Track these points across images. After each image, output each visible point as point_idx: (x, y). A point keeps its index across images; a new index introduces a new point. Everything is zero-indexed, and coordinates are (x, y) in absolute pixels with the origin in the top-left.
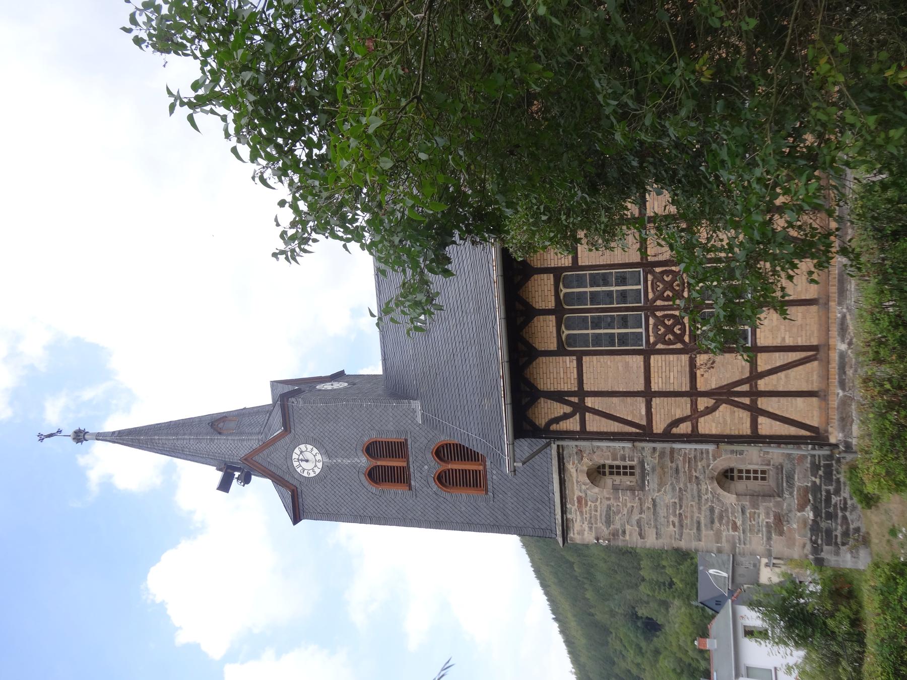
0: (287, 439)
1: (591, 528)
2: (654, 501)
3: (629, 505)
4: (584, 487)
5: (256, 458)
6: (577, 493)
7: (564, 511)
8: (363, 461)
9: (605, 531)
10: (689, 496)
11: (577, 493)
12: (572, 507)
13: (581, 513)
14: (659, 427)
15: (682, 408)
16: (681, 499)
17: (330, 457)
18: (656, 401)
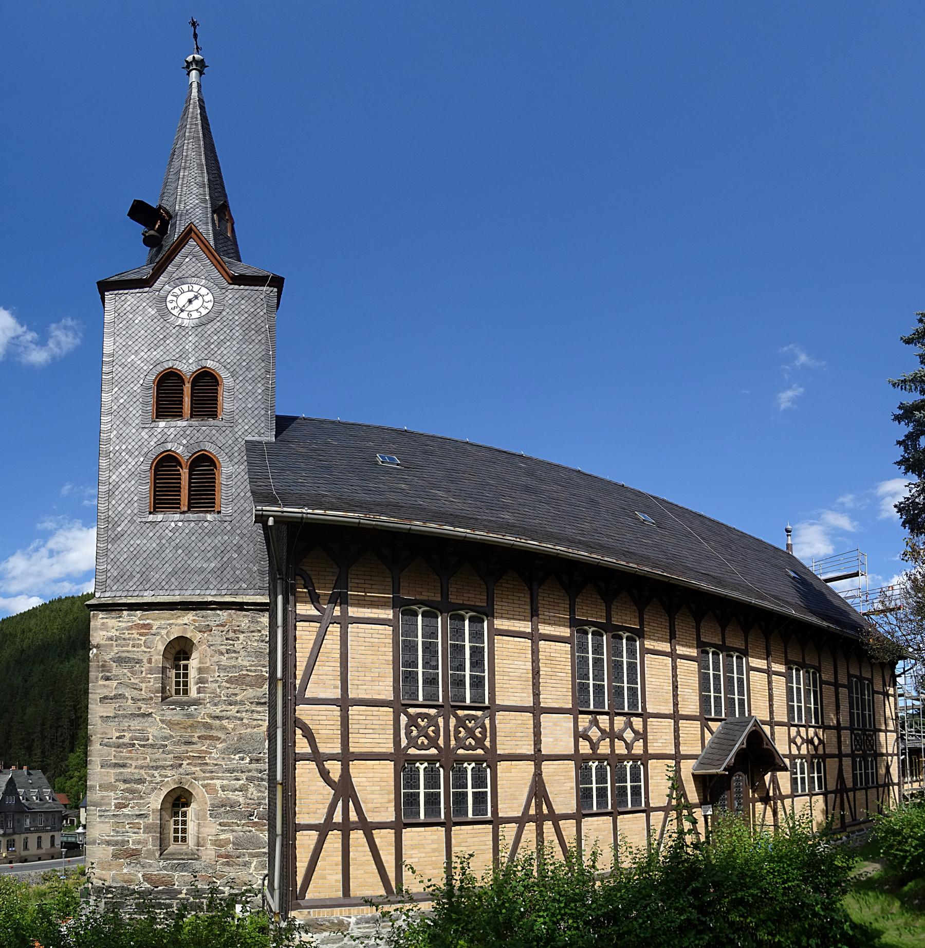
1: (111, 639)
3: (143, 686)
4: (164, 632)
6: (156, 624)
10: (157, 756)
11: (156, 624)
13: (130, 628)
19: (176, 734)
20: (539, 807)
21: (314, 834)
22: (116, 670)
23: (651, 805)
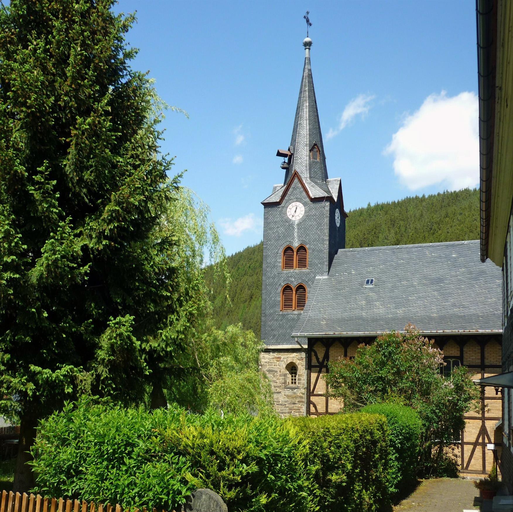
0: (308, 200)
1: (266, 362)
2: (280, 392)
3: (278, 381)
4: (285, 360)
5: (296, 180)
6: (282, 357)
7: (274, 351)
8: (296, 244)
9: (265, 369)
10: (283, 408)
11: (282, 357)
12: (276, 355)
13: (273, 358)
14: (313, 399)
15: (321, 408)
16: (281, 405)
17: (298, 225)
18: (324, 398)
19: (290, 400)
20: (484, 439)
21: (471, 447)
22: (269, 375)
23: (465, 441)
